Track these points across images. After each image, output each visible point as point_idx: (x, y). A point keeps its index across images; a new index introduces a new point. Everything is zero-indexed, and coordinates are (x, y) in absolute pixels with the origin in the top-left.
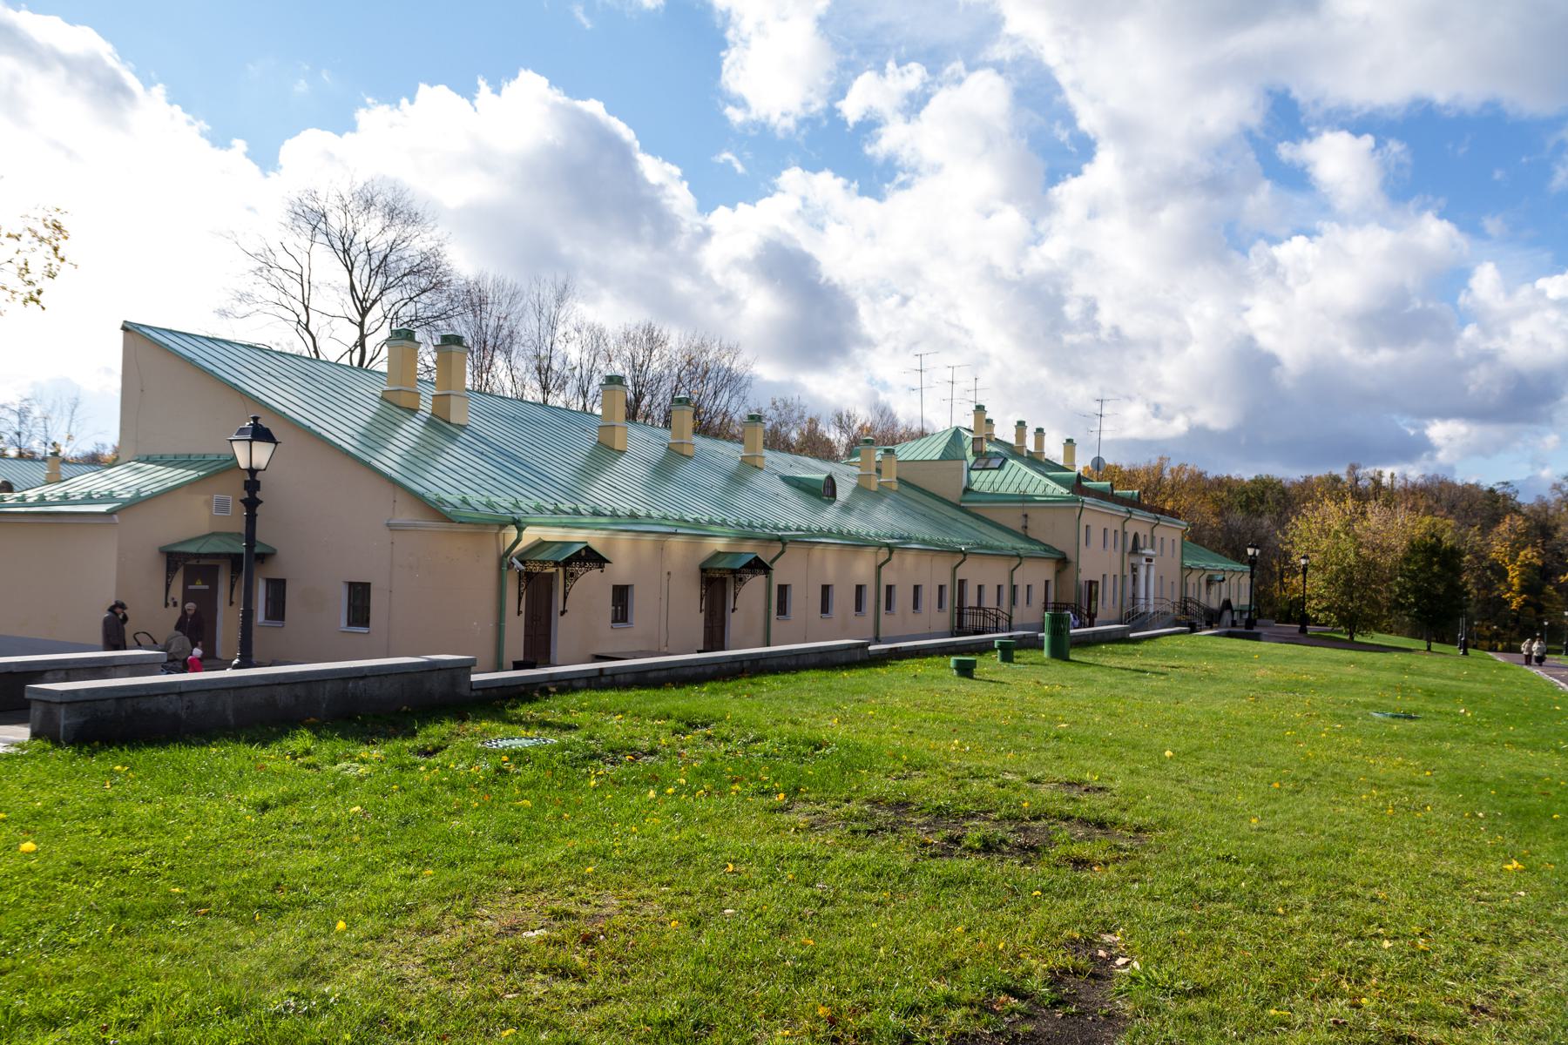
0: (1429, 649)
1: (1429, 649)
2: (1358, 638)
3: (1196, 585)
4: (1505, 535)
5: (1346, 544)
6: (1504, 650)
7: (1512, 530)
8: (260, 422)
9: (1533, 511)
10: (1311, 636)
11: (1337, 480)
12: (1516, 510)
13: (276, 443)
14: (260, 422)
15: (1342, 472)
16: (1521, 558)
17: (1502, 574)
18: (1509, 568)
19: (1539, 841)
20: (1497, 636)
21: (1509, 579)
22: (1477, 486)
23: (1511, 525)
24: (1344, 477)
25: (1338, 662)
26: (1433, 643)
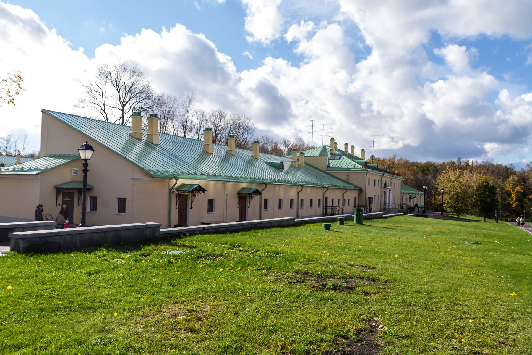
0: (485, 220)
1: (485, 220)
2: (461, 217)
3: (406, 199)
4: (511, 182)
5: (457, 185)
7: (513, 180)
8: (88, 143)
10: (445, 216)
11: (454, 163)
12: (514, 173)
13: (94, 151)
14: (88, 143)
15: (455, 160)
16: (516, 190)
17: (510, 195)
18: (512, 193)
20: (508, 216)
21: (512, 197)
22: (501, 165)
23: (513, 178)
24: (456, 162)
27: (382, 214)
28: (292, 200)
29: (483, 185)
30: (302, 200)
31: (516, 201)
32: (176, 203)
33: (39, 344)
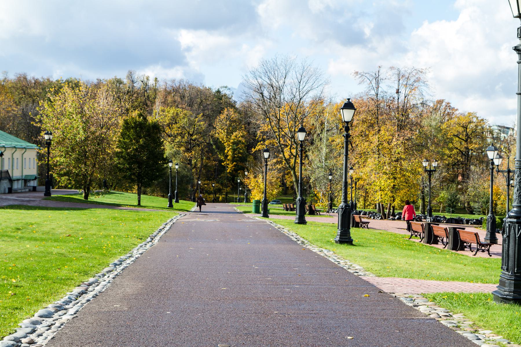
0: (171, 206)
1: (171, 206)
2: (92, 198)
3: (11, 160)
4: (224, 122)
5: (78, 123)
6: (223, 201)
7: (228, 118)
8: (350, 100)
9: (244, 106)
11: (120, 82)
12: (232, 105)
13: (355, 110)
14: (350, 100)
15: (123, 76)
16: (233, 137)
17: (221, 148)
18: (226, 144)
20: (219, 191)
21: (226, 151)
22: (210, 89)
23: (227, 115)
24: (125, 81)
25: (29, 214)
26: (141, 196)
27: (232, 194)
28: (9, 158)
29: (135, 123)
30: (25, 158)
31: (233, 161)
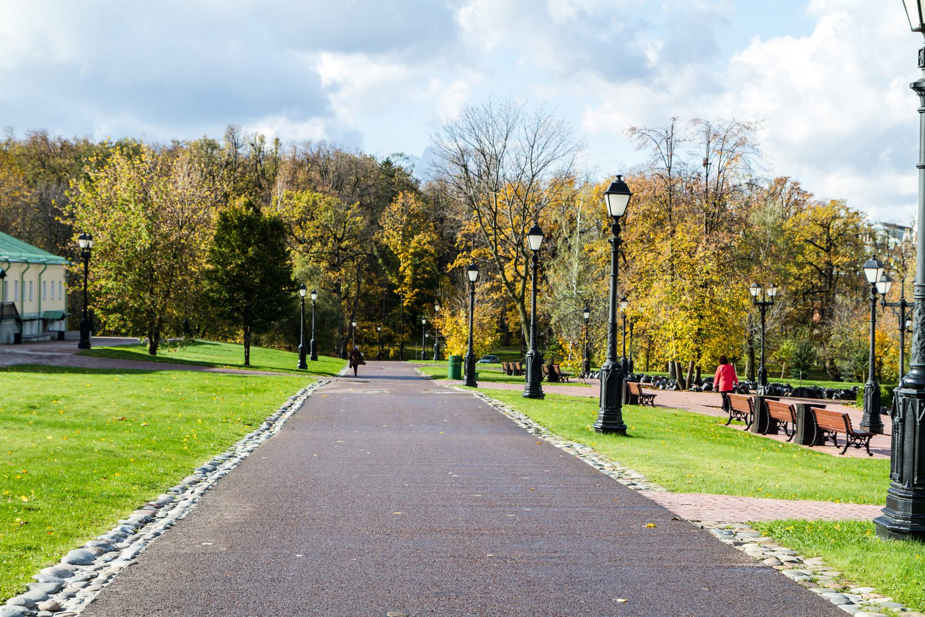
0: (303, 366)
1: (303, 366)
2: (163, 352)
3: (19, 284)
4: (398, 216)
5: (139, 220)
7: (405, 210)
8: (622, 179)
9: (433, 189)
10: (100, 354)
11: (212, 145)
12: (412, 187)
14: (622, 179)
15: (218, 135)
16: (413, 244)
18: (400, 257)
19: (865, 602)
20: (388, 340)
21: (401, 269)
22: (372, 158)
23: (403, 205)
24: (222, 144)
26: (251, 348)
29: (239, 219)
32: (215, 372)
33: (558, 554)
